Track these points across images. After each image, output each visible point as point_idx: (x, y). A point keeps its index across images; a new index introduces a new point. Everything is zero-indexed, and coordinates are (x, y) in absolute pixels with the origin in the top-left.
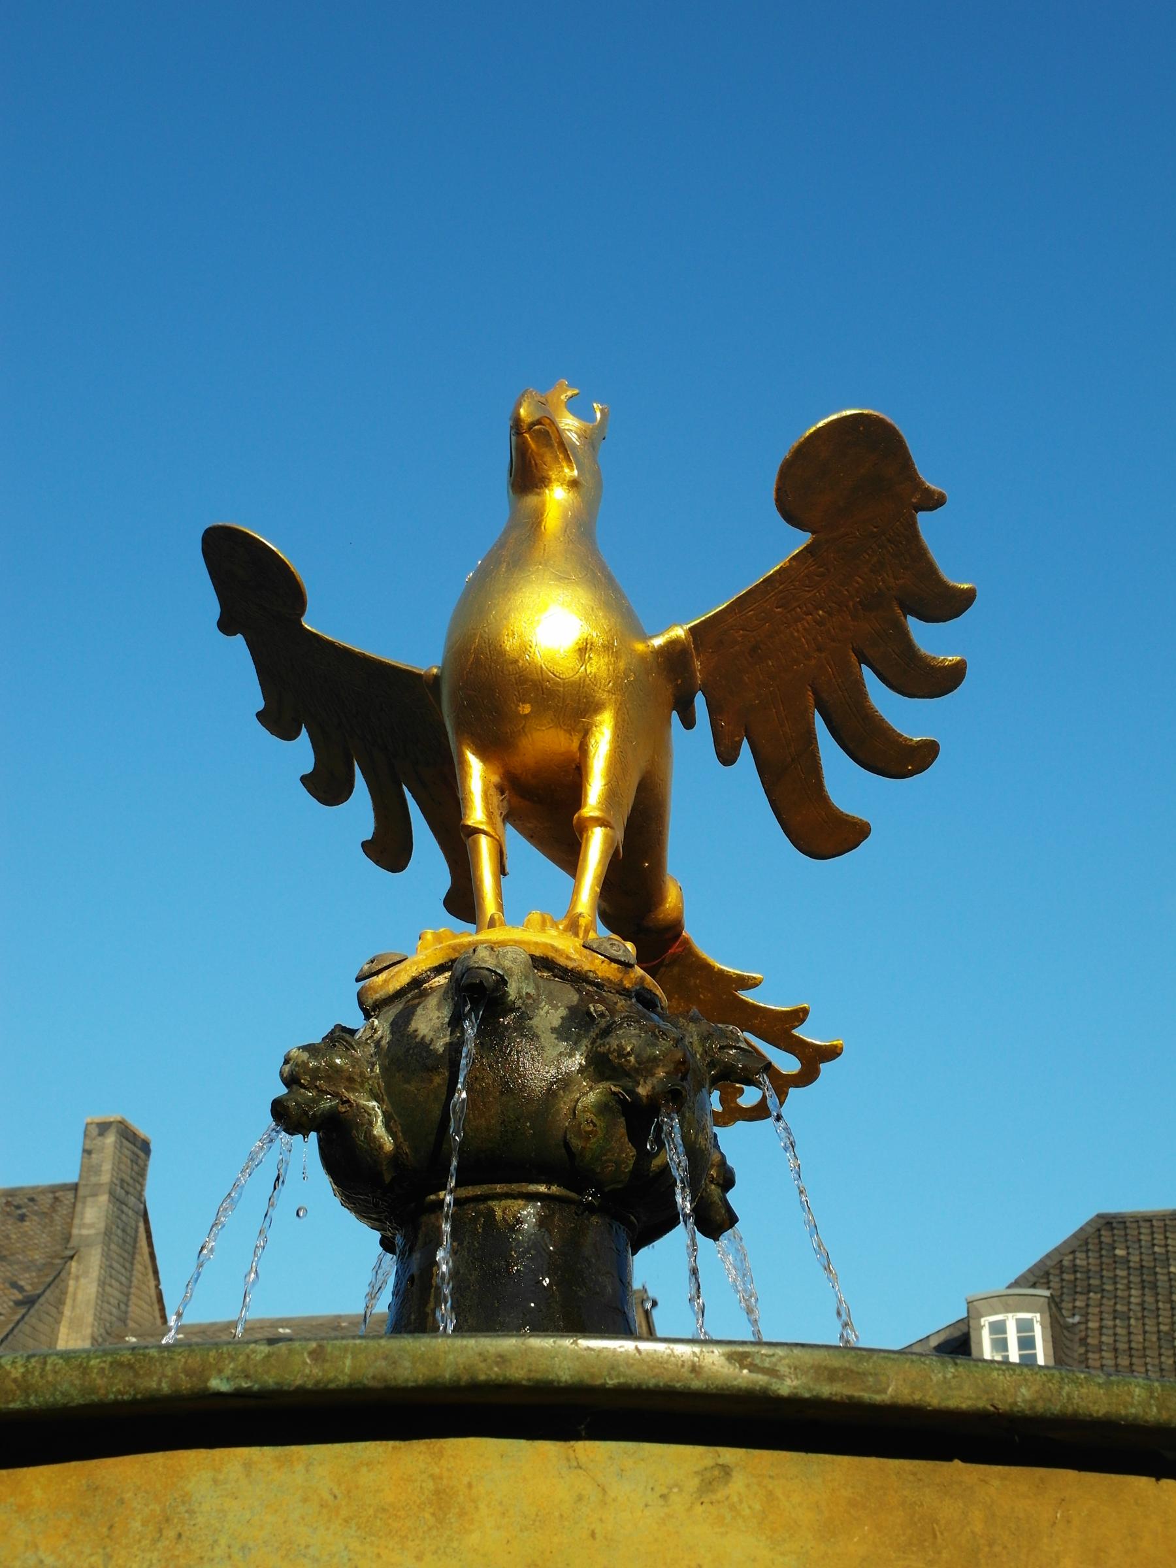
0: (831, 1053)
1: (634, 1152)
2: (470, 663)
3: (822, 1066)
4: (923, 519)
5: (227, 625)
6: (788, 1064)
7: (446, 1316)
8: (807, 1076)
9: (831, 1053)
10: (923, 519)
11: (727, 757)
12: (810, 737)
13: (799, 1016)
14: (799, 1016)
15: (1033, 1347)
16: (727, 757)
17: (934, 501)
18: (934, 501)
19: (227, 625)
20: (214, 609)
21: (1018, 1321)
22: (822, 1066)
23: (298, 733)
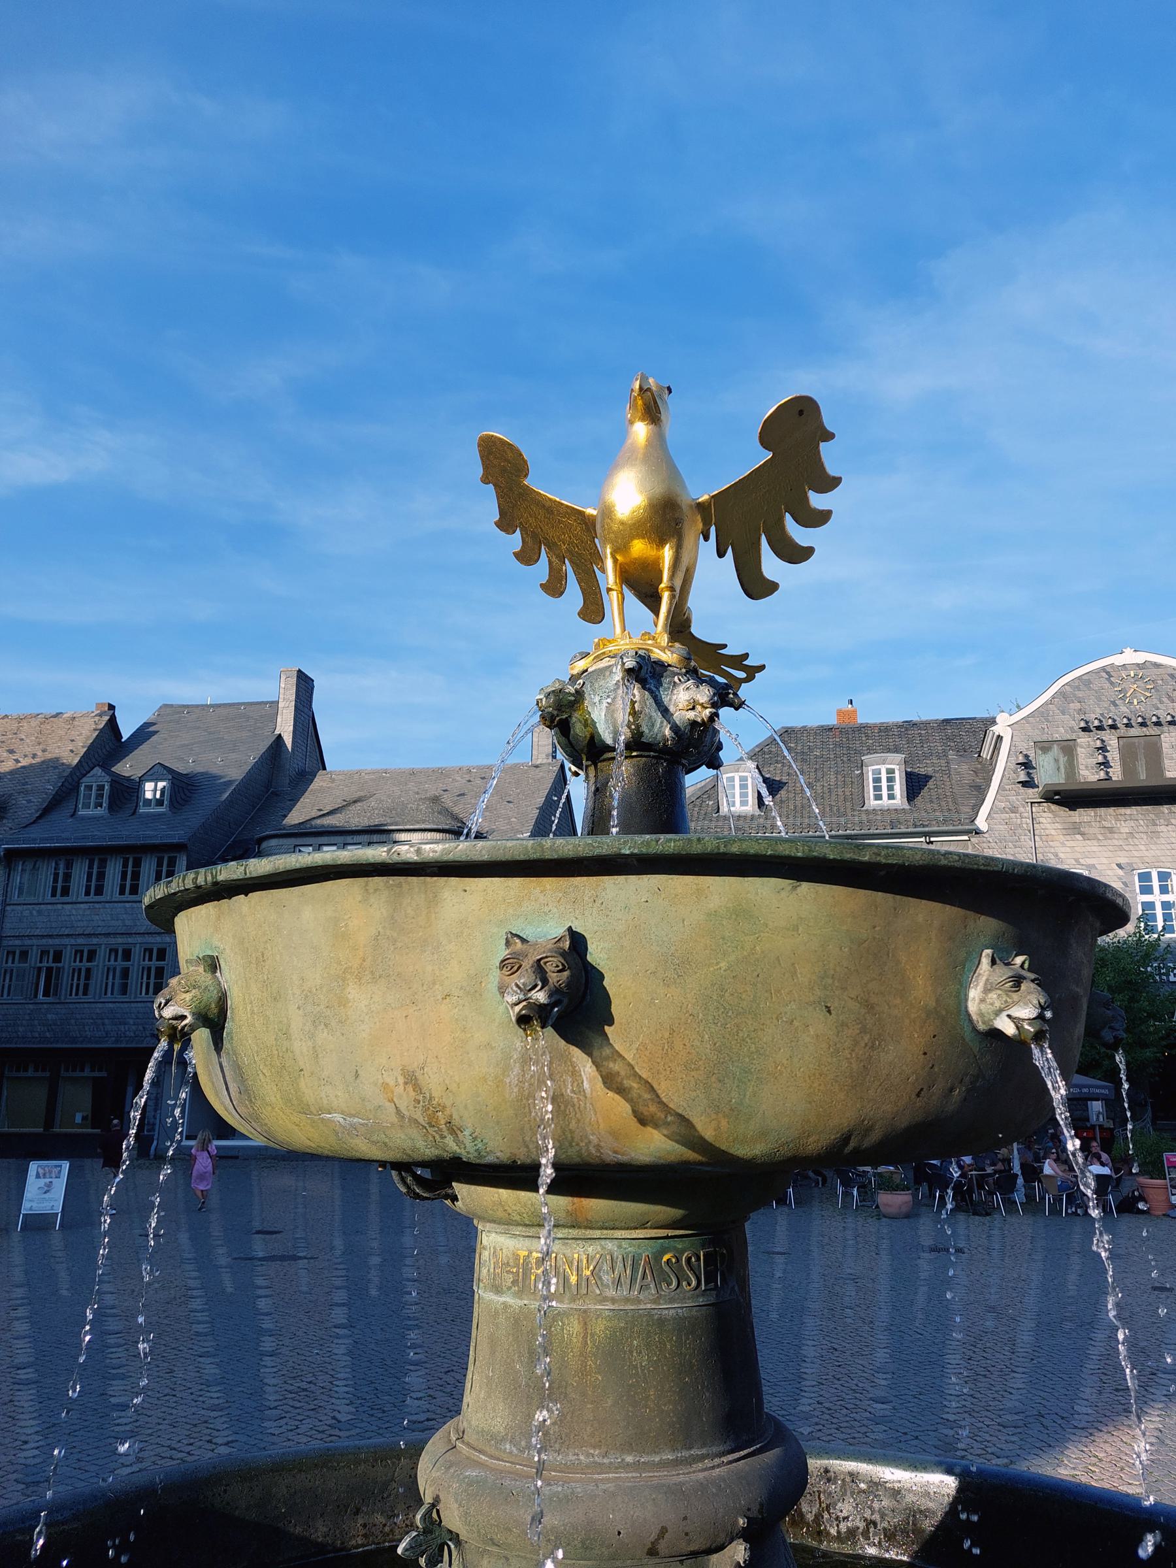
0: (762, 668)
1: (302, 1084)
2: (521, 1261)
3: (756, 674)
4: (822, 446)
5: (485, 480)
6: (741, 675)
7: (70, 1070)
8: (750, 678)
9: (762, 668)
10: (822, 446)
11: (721, 554)
12: (759, 539)
13: (746, 656)
14: (746, 656)
15: (874, 787)
16: (721, 554)
17: (829, 436)
18: (829, 436)
19: (485, 480)
20: (480, 471)
21: (169, 857)
22: (756, 674)
23: (514, 532)
